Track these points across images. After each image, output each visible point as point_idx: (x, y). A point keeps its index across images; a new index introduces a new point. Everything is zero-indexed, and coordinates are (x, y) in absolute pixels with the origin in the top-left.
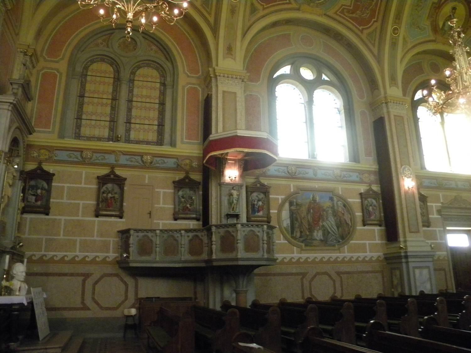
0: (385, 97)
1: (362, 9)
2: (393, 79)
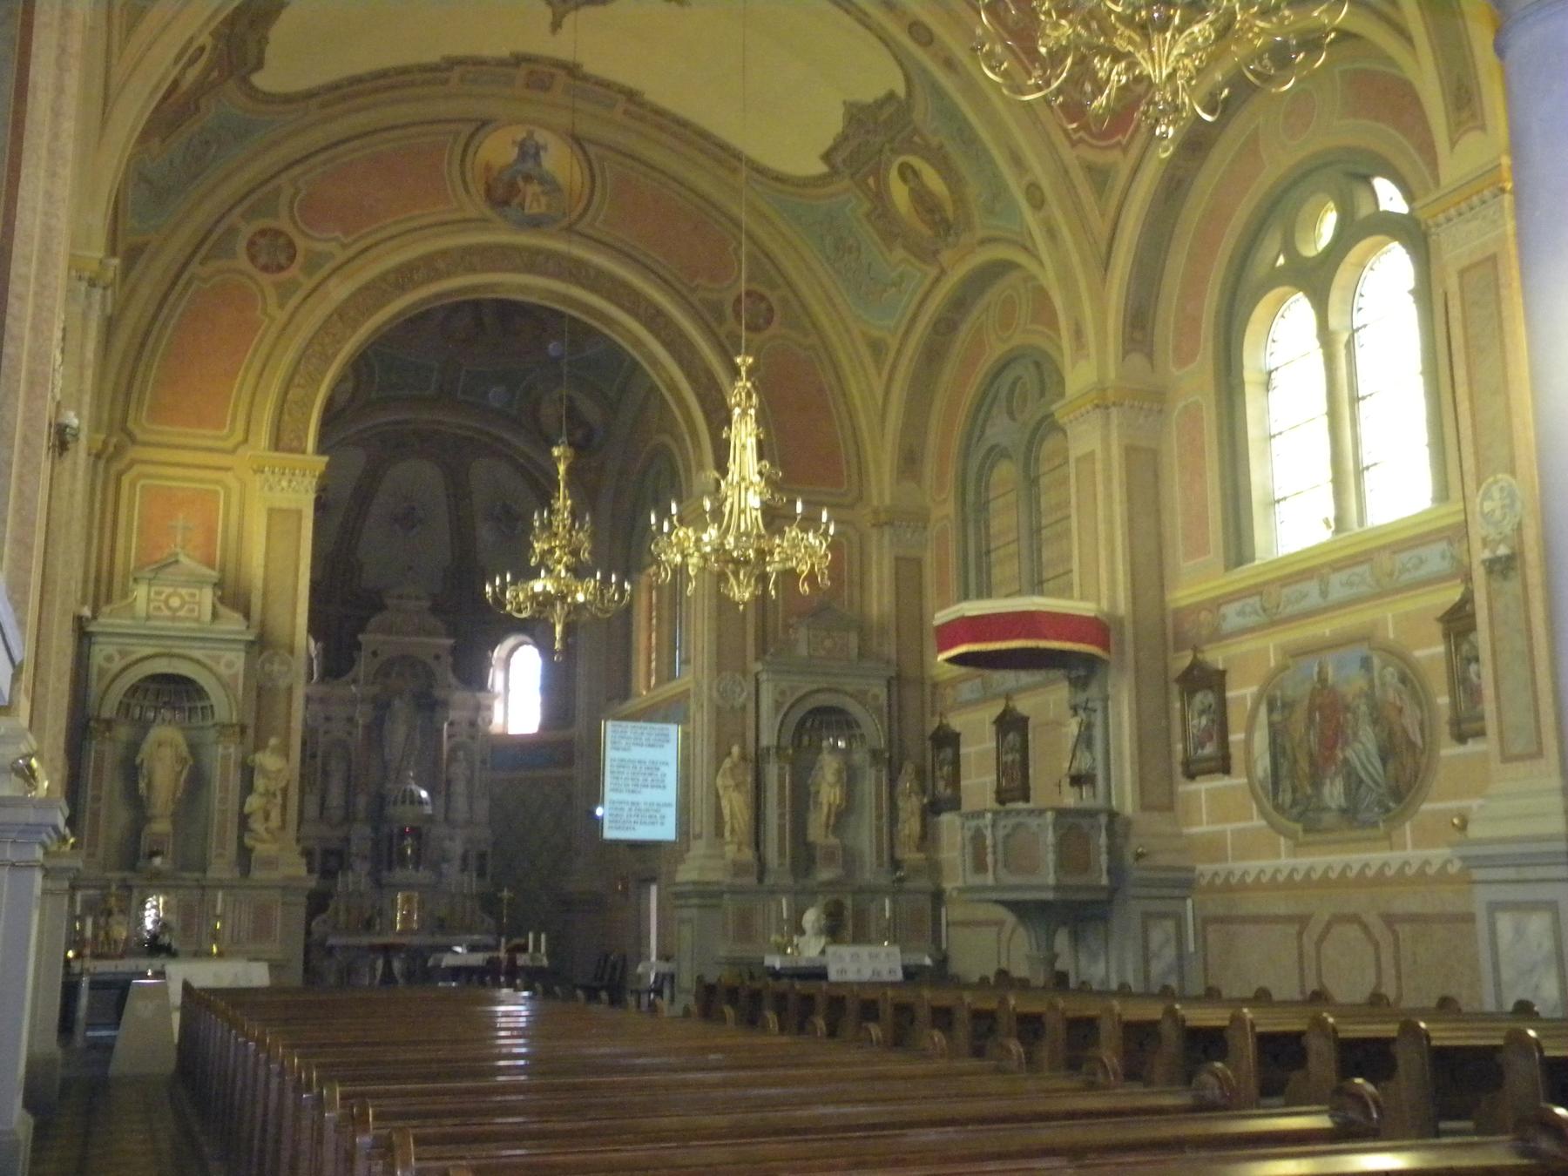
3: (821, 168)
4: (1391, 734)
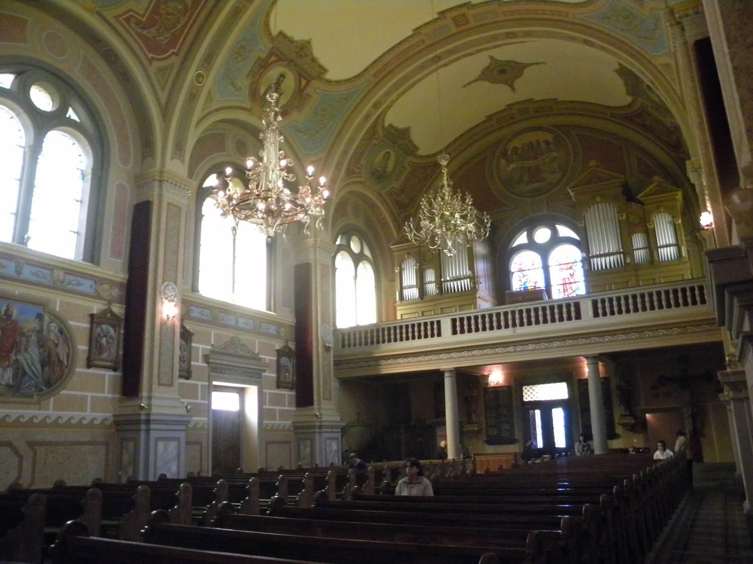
0: (161, 172)
1: (161, 28)
2: (179, 147)
3: (274, 31)
4: (49, 356)
